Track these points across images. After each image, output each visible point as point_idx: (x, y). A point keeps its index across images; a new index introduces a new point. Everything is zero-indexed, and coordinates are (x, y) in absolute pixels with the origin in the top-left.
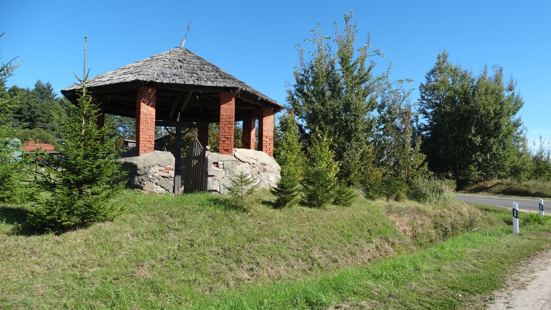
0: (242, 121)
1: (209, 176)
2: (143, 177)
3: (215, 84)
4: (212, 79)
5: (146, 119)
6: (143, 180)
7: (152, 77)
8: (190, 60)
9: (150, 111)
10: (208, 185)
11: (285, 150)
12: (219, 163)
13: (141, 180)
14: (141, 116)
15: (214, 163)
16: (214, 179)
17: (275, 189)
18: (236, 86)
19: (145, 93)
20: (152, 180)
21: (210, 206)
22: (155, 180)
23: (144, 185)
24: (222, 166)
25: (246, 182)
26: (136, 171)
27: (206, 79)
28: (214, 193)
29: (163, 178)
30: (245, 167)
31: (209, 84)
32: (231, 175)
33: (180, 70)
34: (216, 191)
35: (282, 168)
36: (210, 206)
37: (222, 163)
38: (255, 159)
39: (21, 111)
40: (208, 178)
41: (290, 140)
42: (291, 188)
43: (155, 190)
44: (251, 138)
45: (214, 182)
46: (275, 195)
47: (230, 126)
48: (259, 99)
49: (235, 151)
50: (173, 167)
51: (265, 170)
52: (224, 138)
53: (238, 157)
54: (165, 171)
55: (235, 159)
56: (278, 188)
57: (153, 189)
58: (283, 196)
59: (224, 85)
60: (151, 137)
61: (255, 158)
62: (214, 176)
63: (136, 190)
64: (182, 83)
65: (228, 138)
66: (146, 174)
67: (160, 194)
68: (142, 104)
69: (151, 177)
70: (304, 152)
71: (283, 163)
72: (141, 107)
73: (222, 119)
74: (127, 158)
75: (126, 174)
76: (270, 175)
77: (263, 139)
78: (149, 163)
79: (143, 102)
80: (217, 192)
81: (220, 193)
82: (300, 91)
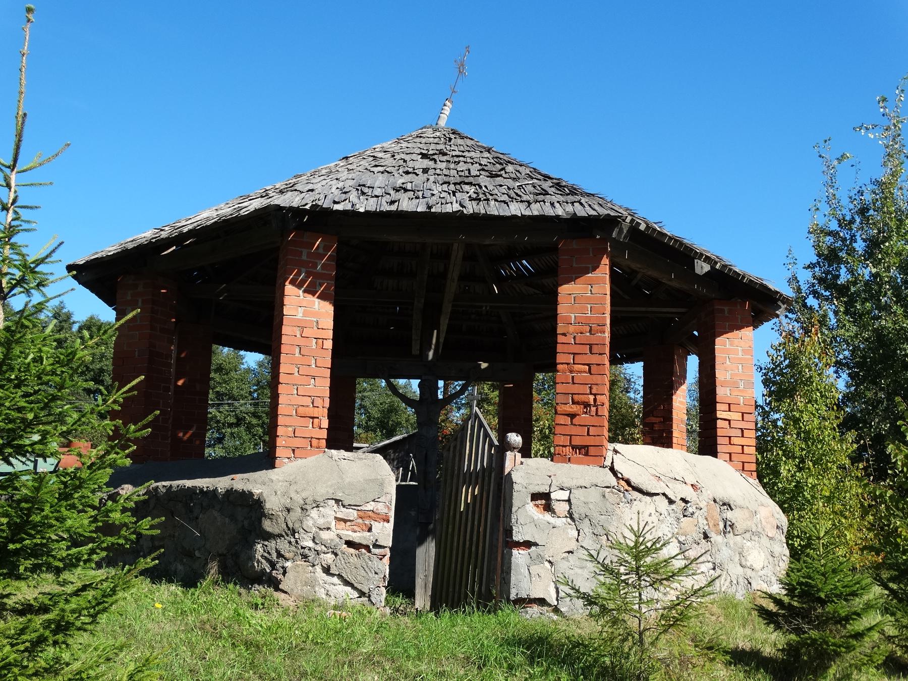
0: (640, 365)
1: (518, 545)
2: (283, 545)
3: (536, 210)
4: (525, 198)
5: (302, 342)
6: (283, 556)
7: (322, 196)
8: (461, 154)
9: (315, 314)
10: (513, 578)
11: (794, 458)
12: (553, 496)
13: (274, 555)
14: (285, 330)
15: (535, 497)
16: (534, 556)
17: (778, 602)
18: (613, 214)
19: (301, 252)
20: (312, 555)
21: (511, 667)
22: (322, 555)
23: (284, 573)
24: (566, 506)
25: (656, 571)
26: (260, 522)
27: (505, 198)
28: (535, 609)
29: (352, 551)
30: (653, 512)
31: (516, 209)
32: (598, 542)
33: (422, 177)
34: (542, 602)
35: (791, 524)
36: (511, 667)
37: (564, 495)
38: (689, 482)
39: (100, 376)
40: (515, 552)
41: (810, 422)
42: (846, 600)
43: (321, 594)
44: (675, 416)
45: (535, 569)
46: (778, 627)
47: (594, 359)
48: (702, 268)
49: (616, 452)
50: (386, 511)
51: (729, 527)
52: (574, 403)
53: (626, 476)
54: (358, 525)
55: (613, 481)
56: (786, 600)
57: (313, 587)
58: (814, 634)
59: (567, 213)
60: (318, 402)
61: (691, 480)
62: (536, 544)
63: (258, 590)
64: (420, 209)
65: (586, 405)
66: (294, 532)
67: (336, 608)
68: (289, 289)
69: (310, 544)
70: (861, 466)
71: (790, 505)
72: (287, 300)
73: (564, 335)
74: (238, 476)
75: (152, 527)
76: (749, 544)
77: (720, 414)
78: (304, 495)
79: (293, 283)
80: (545, 608)
81: (556, 610)
82: (828, 282)
